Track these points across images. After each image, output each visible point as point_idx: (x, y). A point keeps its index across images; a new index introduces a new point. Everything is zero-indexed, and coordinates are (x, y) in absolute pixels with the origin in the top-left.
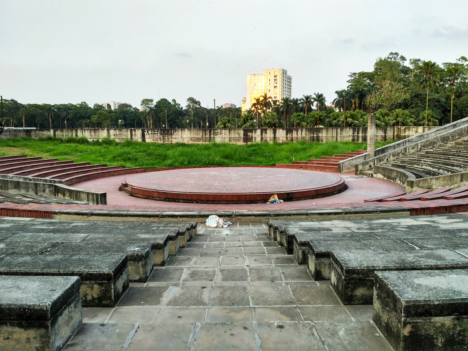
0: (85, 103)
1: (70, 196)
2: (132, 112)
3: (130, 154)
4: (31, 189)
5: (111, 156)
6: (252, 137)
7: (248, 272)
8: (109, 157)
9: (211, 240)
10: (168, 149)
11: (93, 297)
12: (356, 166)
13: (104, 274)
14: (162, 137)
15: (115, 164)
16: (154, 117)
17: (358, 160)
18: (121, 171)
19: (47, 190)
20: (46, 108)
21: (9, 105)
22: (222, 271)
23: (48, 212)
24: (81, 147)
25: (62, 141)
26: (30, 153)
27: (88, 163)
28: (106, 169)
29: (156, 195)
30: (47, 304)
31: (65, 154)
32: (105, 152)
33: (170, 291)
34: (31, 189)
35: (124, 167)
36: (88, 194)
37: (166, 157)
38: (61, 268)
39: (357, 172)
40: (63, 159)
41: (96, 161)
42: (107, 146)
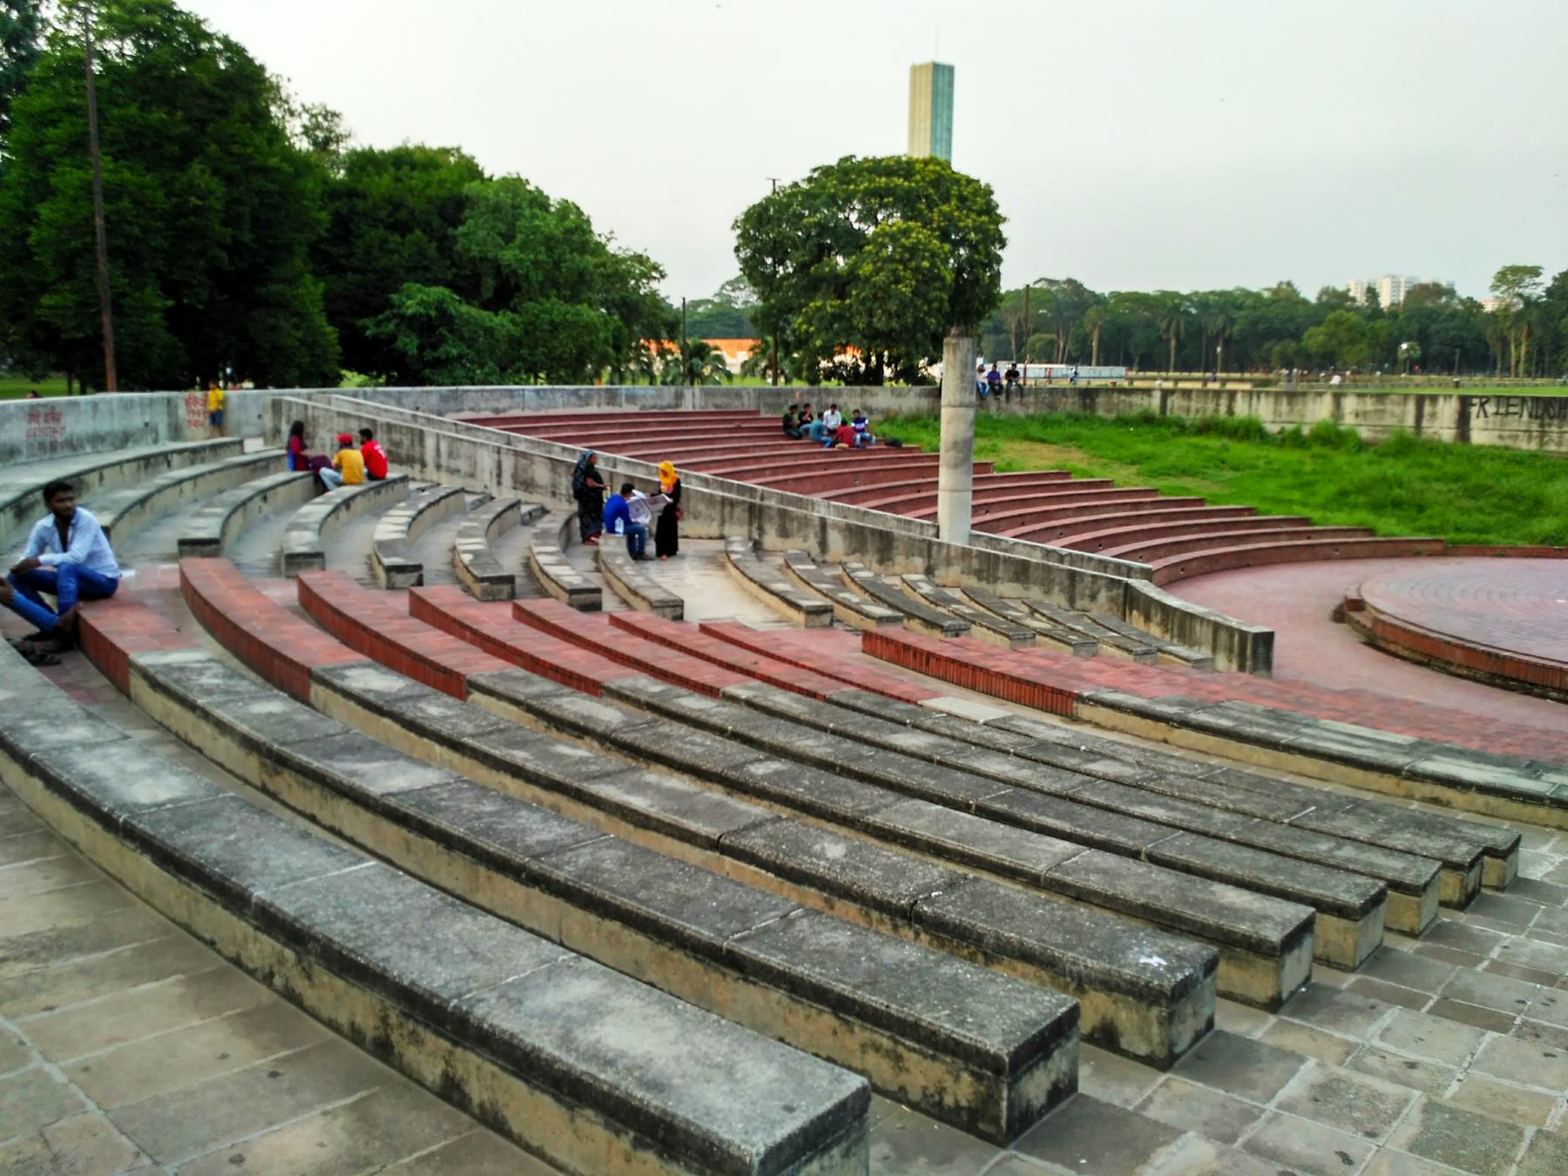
0: (1289, 284)
1: (1164, 624)
2: (1454, 315)
3: (1400, 485)
4: (1057, 588)
5: (1332, 489)
7: (1525, 1144)
8: (1327, 490)
9: (1544, 921)
10: (1552, 478)
11: (957, 1101)
13: (987, 1052)
14: (1535, 427)
15: (1340, 519)
16: (1538, 332)
18: (1357, 548)
19: (1103, 596)
20: (1167, 304)
21: (1060, 296)
23: (1061, 692)
24: (1240, 450)
25: (1181, 428)
26: (1083, 466)
27: (1251, 511)
28: (1308, 535)
29: (1459, 656)
30: (754, 1151)
31: (1185, 472)
32: (1315, 472)
33: (1180, 1148)
34: (1057, 588)
35: (1370, 531)
36: (1217, 627)
37: (1537, 506)
38: (895, 1000)
40: (1174, 490)
41: (1277, 501)
42: (1326, 451)
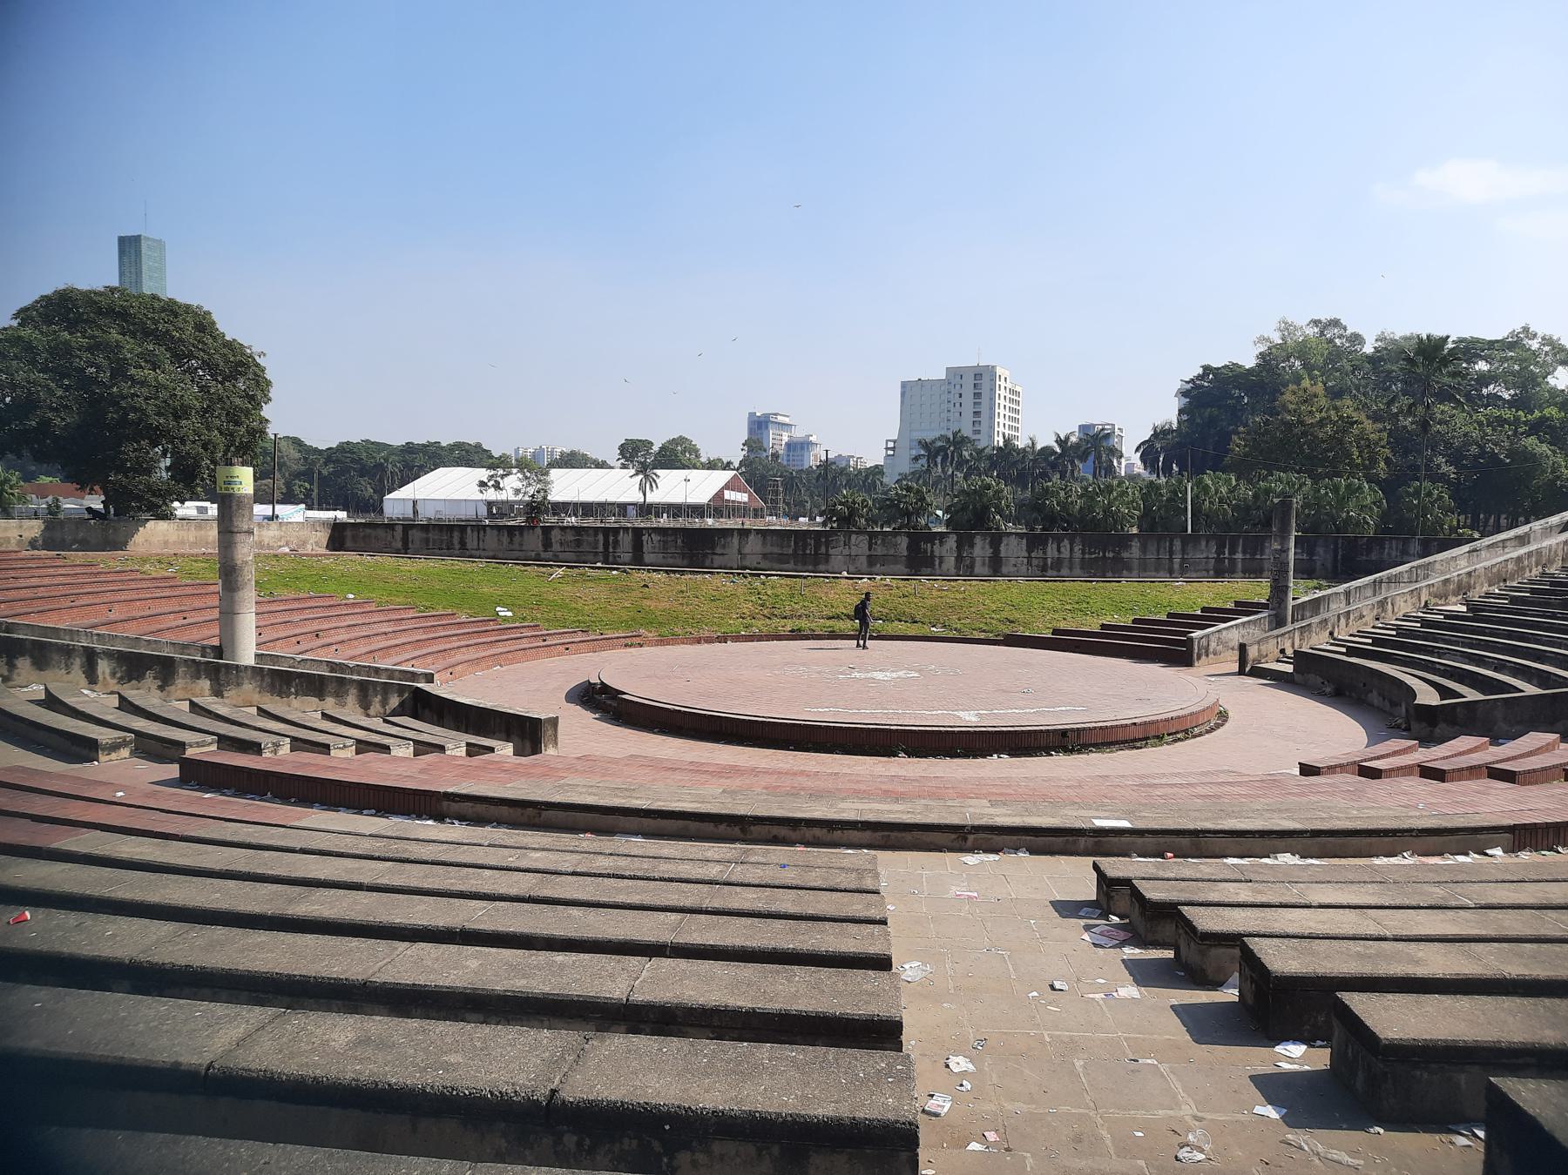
6: (933, 556)
12: (1243, 648)
39: (1248, 668)
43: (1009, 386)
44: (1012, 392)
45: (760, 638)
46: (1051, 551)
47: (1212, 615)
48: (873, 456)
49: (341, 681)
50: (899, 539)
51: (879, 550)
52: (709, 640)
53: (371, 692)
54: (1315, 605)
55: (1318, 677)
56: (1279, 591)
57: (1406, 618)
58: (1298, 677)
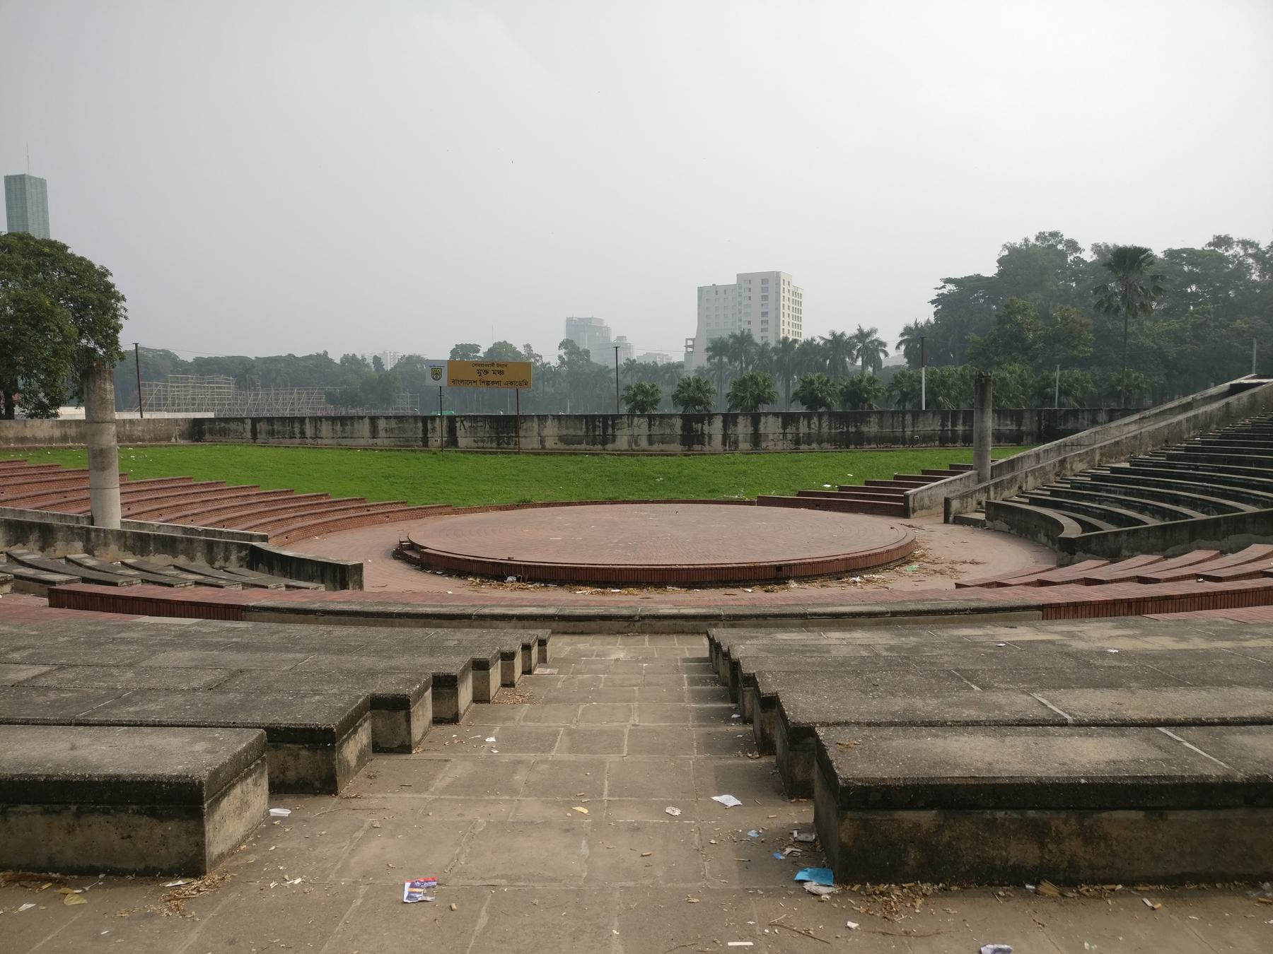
6: (703, 434)
12: (947, 502)
17: (952, 488)
19: (233, 557)
22: (570, 733)
39: (951, 517)
43: (792, 289)
44: (795, 294)
45: (575, 504)
46: (803, 428)
47: (931, 475)
48: (678, 357)
49: (190, 541)
50: (674, 420)
51: (657, 430)
52: (500, 508)
53: (215, 550)
54: (1011, 464)
55: (1009, 521)
56: (981, 456)
57: (1082, 474)
58: (989, 524)
